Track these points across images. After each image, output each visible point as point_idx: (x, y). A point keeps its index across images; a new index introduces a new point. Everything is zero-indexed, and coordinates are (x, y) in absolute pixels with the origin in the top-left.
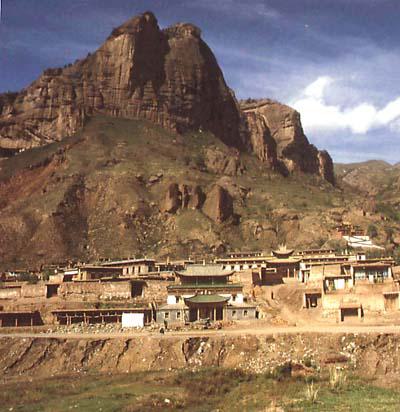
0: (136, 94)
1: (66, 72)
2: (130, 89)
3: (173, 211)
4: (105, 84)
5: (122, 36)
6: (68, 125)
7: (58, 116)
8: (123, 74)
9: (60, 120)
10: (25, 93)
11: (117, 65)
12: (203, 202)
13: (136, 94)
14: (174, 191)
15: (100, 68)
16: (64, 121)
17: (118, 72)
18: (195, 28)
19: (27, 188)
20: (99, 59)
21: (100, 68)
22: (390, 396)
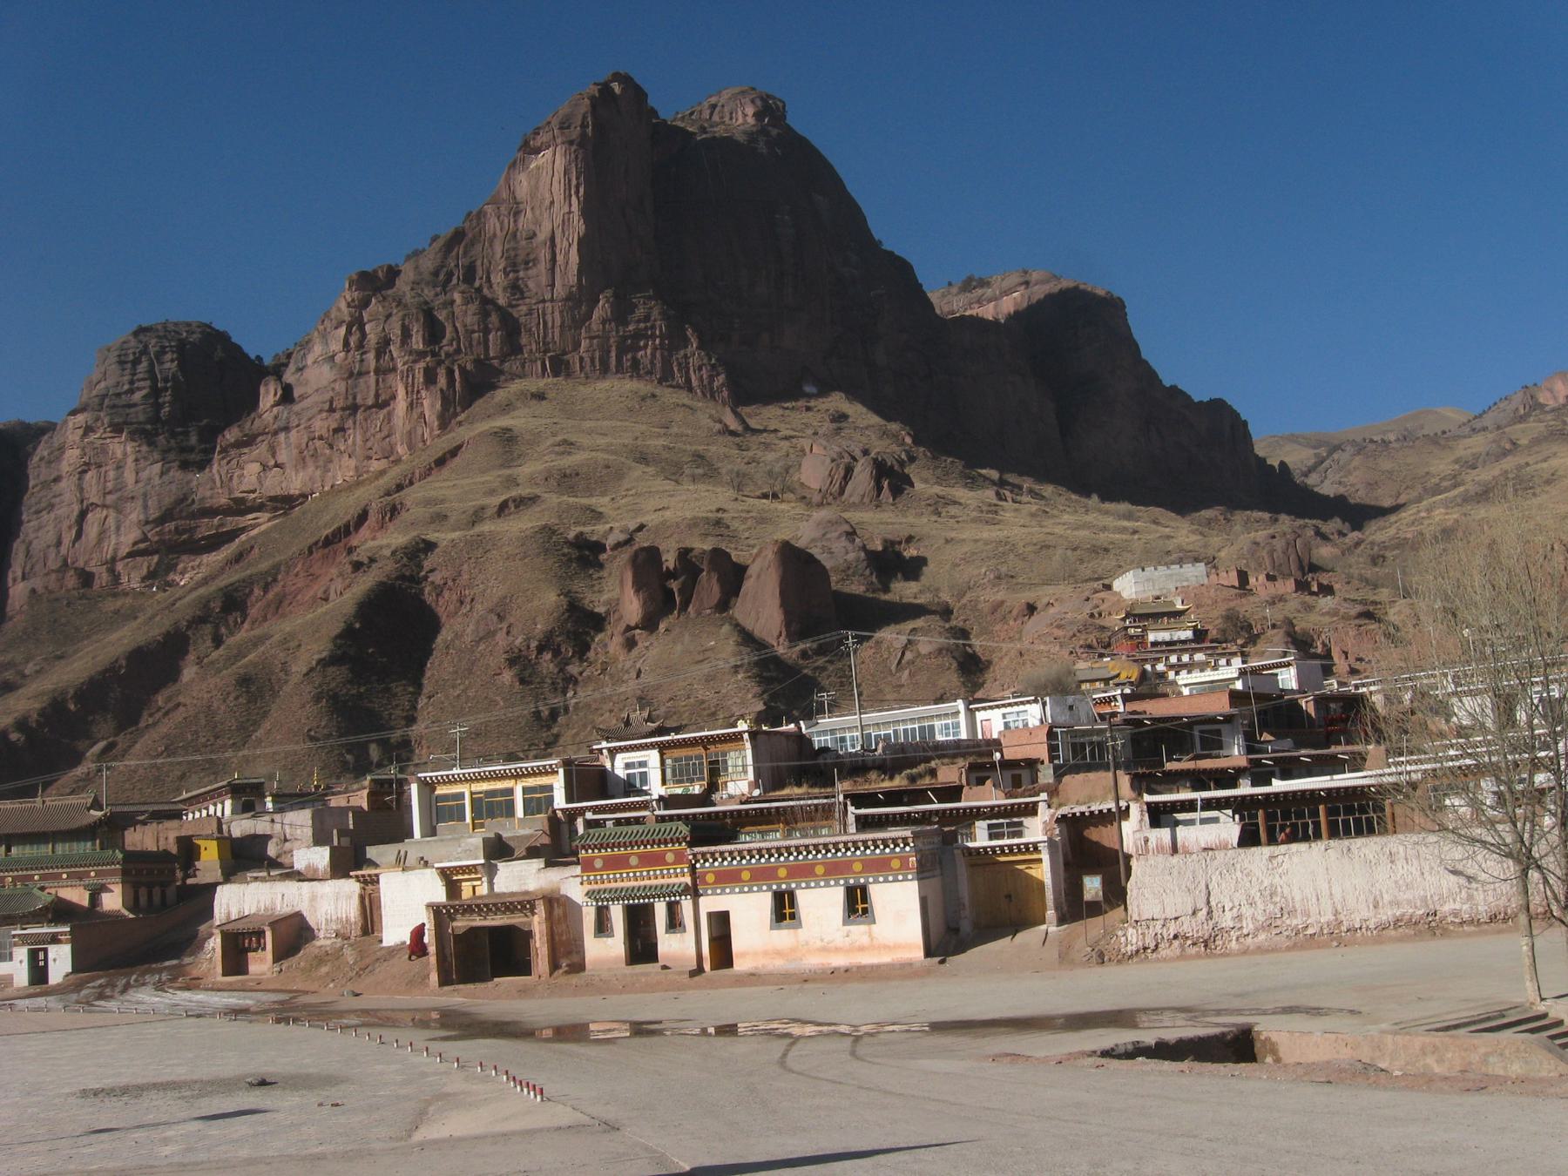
0: (602, 309)
1: (408, 274)
2: (582, 300)
3: (649, 623)
4: (516, 288)
5: (548, 153)
6: (422, 415)
7: (394, 397)
8: (560, 258)
9: (401, 404)
10: (305, 345)
11: (543, 235)
12: (736, 593)
13: (602, 309)
14: (647, 565)
15: (498, 249)
16: (411, 406)
17: (544, 254)
18: (765, 98)
19: (992, 721)
20: (492, 224)
21: (498, 249)
22: (117, 612)
